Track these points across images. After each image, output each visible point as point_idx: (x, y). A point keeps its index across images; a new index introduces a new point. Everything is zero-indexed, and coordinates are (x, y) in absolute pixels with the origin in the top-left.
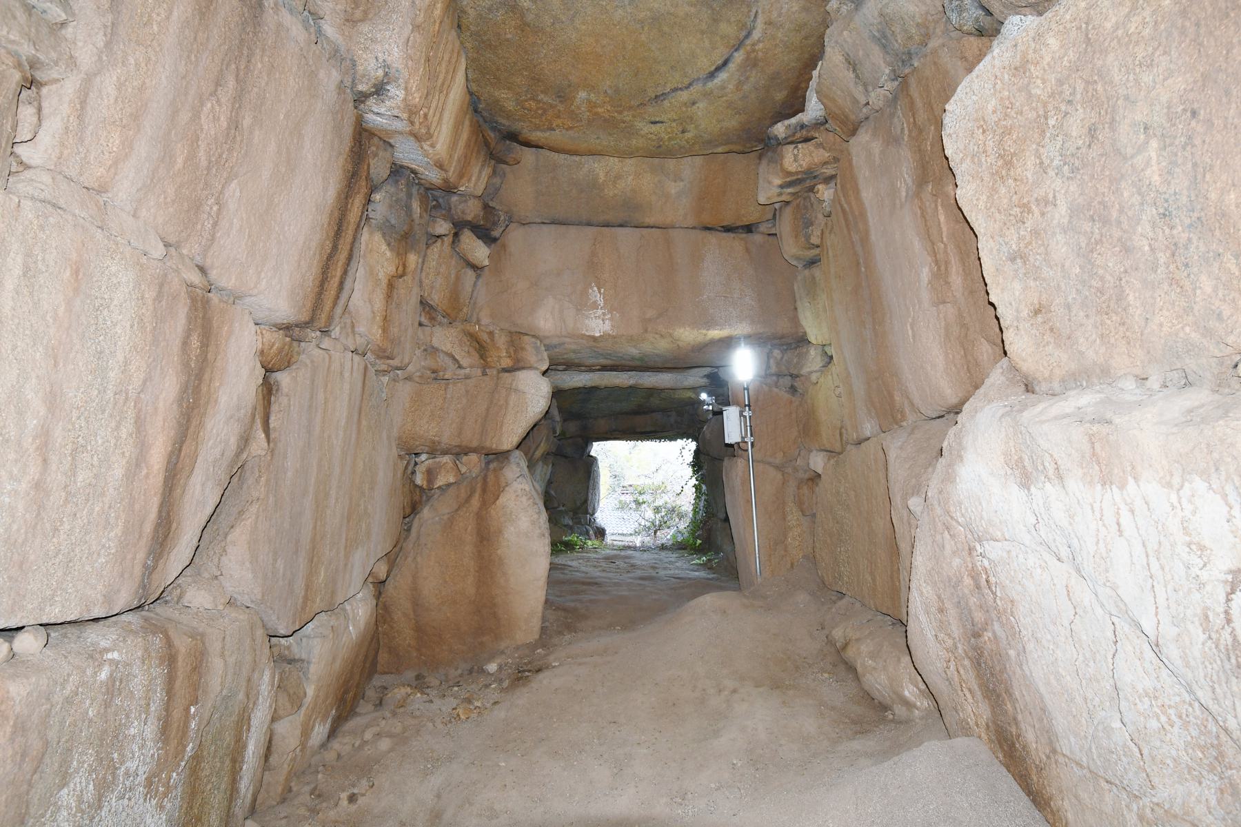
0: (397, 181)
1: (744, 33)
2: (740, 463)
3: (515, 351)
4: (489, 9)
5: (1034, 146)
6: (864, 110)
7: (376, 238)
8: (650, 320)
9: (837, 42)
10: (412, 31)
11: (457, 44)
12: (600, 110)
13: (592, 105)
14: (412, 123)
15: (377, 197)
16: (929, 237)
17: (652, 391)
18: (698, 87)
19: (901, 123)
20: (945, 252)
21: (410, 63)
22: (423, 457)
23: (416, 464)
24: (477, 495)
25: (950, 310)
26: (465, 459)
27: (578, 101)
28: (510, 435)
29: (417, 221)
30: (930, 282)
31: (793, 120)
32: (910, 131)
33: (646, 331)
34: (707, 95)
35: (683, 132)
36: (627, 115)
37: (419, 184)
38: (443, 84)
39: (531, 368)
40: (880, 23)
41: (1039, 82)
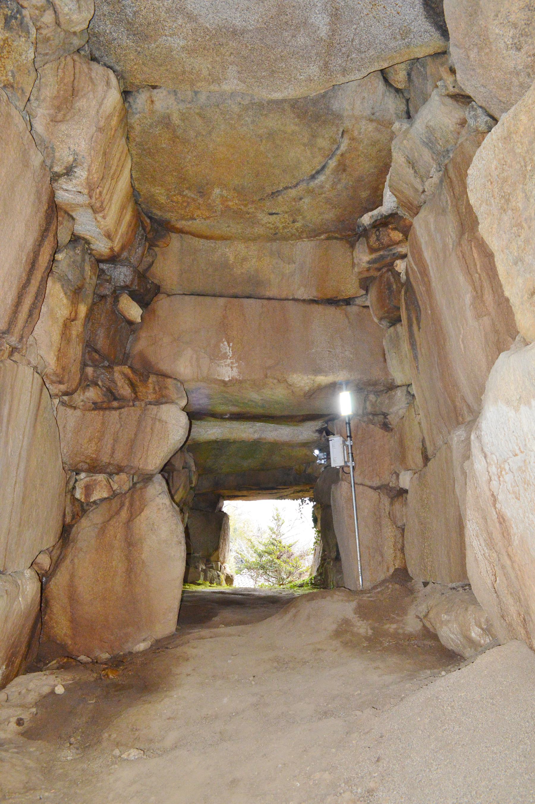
0: (75, 248)
1: (335, 147)
2: (344, 485)
3: (160, 389)
4: (150, 126)
5: (521, 186)
6: (423, 196)
7: (57, 287)
8: (269, 368)
9: (399, 148)
10: (96, 131)
11: (126, 148)
12: (230, 203)
13: (224, 199)
14: (91, 197)
15: (60, 256)
16: (468, 272)
17: (275, 446)
18: (303, 186)
19: (446, 197)
20: (480, 278)
21: (92, 152)
22: (83, 475)
23: (76, 481)
24: (125, 508)
25: (486, 320)
26: (116, 478)
27: (213, 196)
28: (154, 459)
29: (88, 280)
30: (472, 304)
31: (375, 212)
32: (452, 202)
33: (266, 376)
34: (310, 192)
35: (294, 222)
36: (251, 208)
37: (90, 254)
38: (114, 174)
39: (172, 402)
40: (427, 132)
41: (519, 144)
